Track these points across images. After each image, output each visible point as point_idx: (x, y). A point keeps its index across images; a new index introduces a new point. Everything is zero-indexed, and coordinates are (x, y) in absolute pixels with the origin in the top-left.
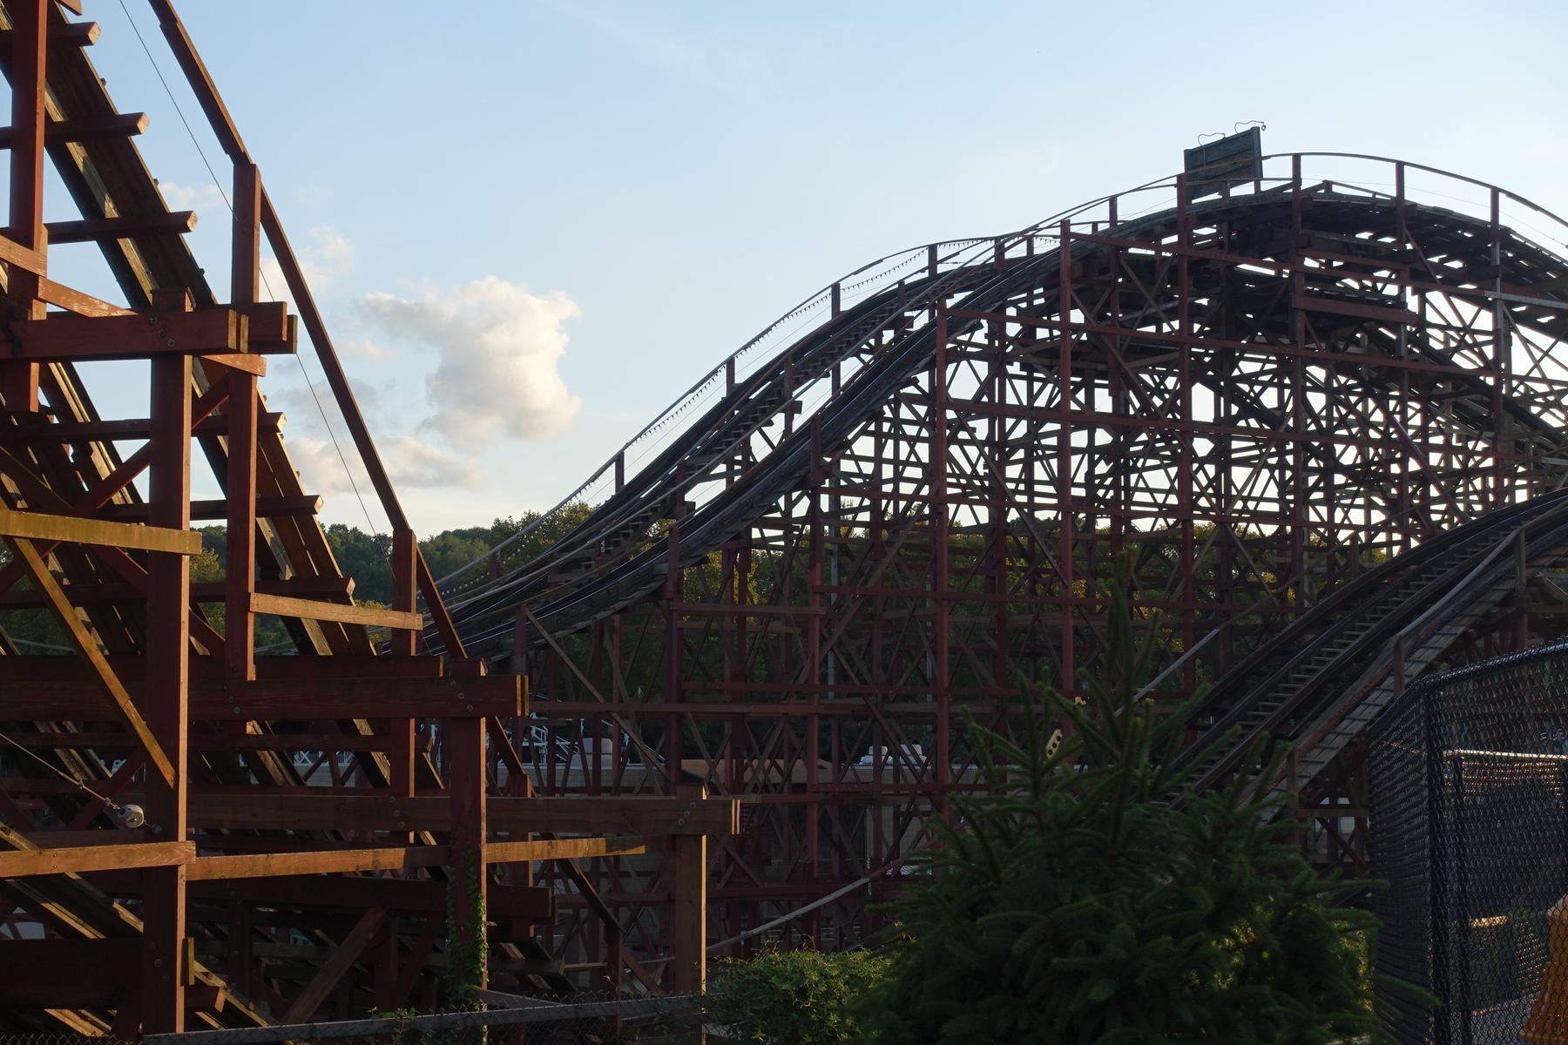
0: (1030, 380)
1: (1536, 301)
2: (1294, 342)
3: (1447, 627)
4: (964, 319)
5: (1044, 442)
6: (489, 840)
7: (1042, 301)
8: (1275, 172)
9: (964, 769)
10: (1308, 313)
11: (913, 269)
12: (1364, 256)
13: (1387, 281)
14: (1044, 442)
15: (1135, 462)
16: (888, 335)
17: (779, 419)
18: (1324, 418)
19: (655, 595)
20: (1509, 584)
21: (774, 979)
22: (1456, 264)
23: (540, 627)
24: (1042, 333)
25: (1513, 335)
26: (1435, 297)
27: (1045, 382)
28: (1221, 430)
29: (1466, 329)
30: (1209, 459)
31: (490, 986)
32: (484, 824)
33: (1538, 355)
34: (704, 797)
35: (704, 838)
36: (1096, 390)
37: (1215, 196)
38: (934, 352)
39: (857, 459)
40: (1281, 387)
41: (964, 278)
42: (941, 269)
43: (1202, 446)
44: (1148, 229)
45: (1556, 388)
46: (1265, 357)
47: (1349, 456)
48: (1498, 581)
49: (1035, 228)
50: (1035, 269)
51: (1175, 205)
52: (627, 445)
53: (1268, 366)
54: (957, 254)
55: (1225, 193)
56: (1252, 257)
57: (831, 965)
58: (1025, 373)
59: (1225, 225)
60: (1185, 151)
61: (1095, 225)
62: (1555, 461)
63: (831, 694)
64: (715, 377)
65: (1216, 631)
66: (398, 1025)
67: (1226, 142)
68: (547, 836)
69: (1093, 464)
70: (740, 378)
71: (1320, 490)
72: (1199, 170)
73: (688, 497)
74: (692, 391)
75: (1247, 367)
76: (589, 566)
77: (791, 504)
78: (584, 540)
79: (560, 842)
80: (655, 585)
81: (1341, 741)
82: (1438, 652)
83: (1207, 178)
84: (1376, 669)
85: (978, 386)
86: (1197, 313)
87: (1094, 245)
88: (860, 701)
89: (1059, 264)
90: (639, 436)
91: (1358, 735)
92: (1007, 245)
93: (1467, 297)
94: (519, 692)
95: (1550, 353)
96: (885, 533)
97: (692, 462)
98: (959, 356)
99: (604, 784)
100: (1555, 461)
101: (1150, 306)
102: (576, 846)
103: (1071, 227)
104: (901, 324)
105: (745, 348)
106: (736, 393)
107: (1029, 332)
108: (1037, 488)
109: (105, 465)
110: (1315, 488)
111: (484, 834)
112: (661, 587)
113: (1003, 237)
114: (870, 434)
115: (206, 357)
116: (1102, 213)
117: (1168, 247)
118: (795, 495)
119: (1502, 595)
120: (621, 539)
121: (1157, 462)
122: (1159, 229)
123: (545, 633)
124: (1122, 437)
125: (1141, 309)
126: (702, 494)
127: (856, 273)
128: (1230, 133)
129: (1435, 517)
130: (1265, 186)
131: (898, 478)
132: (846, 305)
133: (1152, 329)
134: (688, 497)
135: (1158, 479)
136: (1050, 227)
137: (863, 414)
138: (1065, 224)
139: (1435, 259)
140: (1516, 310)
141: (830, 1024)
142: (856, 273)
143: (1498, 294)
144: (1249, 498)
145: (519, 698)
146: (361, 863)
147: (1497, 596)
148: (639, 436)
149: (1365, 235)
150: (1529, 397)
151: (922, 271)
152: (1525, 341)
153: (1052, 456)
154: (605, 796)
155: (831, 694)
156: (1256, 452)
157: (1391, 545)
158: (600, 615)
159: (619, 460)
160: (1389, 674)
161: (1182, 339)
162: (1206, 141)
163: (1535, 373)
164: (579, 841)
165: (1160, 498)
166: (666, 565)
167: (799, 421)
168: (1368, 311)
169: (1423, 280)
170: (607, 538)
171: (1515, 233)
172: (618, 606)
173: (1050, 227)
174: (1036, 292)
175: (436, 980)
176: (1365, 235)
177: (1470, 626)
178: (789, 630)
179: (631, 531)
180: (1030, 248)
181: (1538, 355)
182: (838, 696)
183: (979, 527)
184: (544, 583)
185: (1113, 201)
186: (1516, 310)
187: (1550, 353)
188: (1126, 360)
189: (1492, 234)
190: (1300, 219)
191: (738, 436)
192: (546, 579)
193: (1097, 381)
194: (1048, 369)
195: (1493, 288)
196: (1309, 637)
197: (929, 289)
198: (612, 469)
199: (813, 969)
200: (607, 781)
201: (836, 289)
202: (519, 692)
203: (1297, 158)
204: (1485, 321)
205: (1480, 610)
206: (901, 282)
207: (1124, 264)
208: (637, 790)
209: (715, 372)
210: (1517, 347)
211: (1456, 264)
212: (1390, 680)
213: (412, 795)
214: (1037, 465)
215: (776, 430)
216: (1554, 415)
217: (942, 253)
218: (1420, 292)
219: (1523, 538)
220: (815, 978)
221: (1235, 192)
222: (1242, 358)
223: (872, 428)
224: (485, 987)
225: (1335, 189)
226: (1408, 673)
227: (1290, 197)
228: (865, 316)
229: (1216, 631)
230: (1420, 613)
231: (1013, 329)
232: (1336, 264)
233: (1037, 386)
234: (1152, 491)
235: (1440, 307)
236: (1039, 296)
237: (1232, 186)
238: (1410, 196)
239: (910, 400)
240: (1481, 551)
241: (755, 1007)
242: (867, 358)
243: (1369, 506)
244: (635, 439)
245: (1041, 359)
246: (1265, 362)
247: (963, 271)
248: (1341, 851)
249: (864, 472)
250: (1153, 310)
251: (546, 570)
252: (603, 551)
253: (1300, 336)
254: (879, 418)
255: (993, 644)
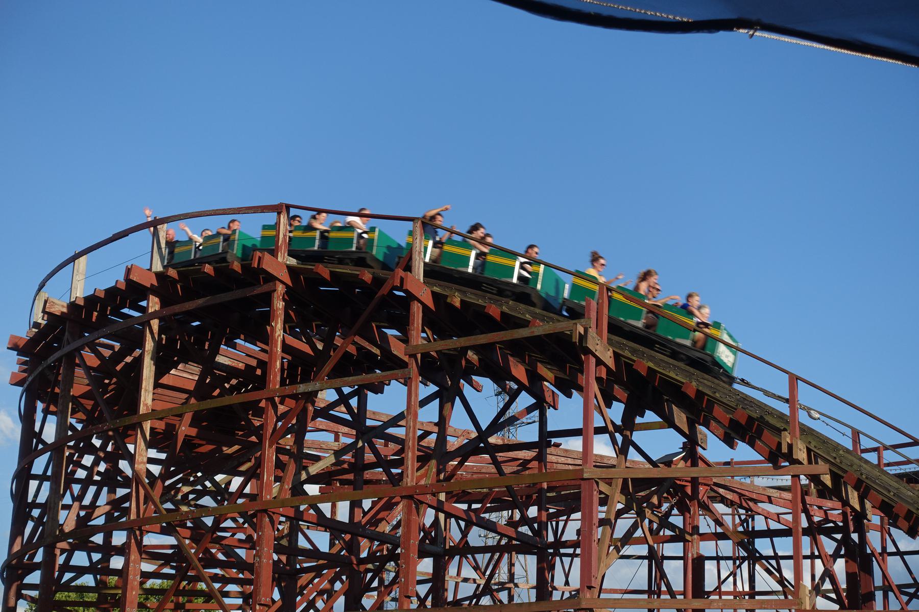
95: (646, 588)
103: (745, 590)
109: (702, 354)
115: (518, 543)
124: (82, 444)
187: (646, 588)
193: (653, 589)
248: (72, 443)
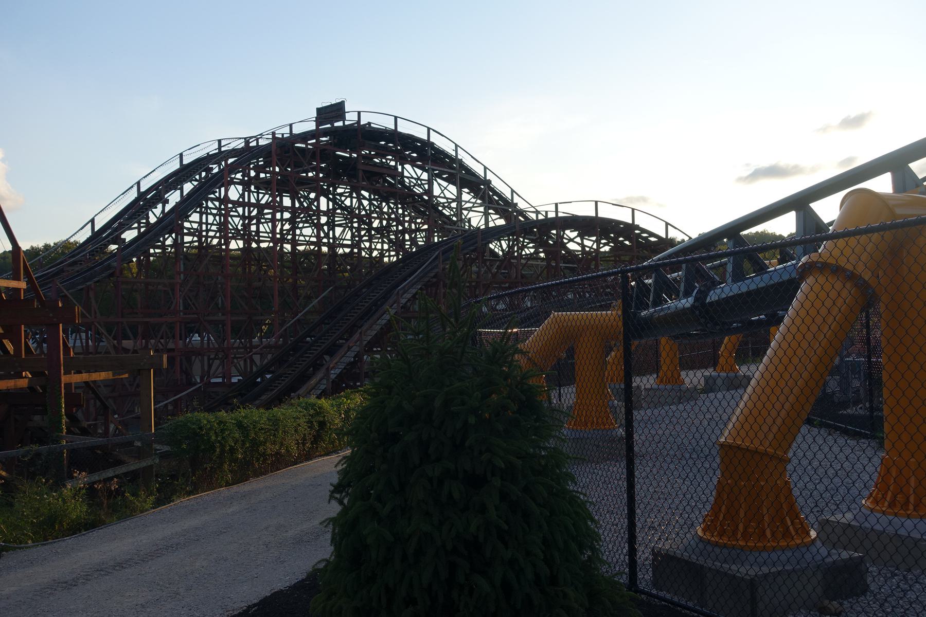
0: (258, 193)
1: (442, 169)
2: (358, 181)
3: (415, 286)
4: (233, 169)
5: (266, 216)
6: (65, 374)
7: (262, 163)
8: (351, 118)
9: (235, 342)
10: (363, 170)
11: (212, 149)
12: (383, 150)
13: (391, 160)
14: (266, 216)
15: (298, 225)
16: (204, 174)
17: (160, 206)
18: (361, 209)
19: (112, 275)
20: (436, 270)
21: (189, 424)
22: (415, 155)
23: (62, 288)
24: (262, 175)
25: (435, 182)
26: (408, 166)
27: (265, 194)
28: (330, 213)
29: (418, 179)
30: (326, 224)
31: (66, 433)
32: (62, 368)
33: (443, 188)
34: (152, 354)
35: (152, 370)
36: (284, 197)
37: (329, 126)
38: (223, 181)
39: (191, 222)
40: (352, 198)
41: (233, 152)
42: (223, 149)
43: (324, 220)
44: (304, 137)
45: (449, 200)
46: (345, 187)
47: (376, 224)
48: (431, 269)
49: (261, 134)
50: (262, 150)
51: (315, 128)
52: (96, 215)
53: (347, 190)
54: (230, 143)
55: (332, 125)
56: (343, 149)
57: (211, 417)
58: (256, 190)
59: (332, 137)
60: (317, 108)
61: (283, 135)
62: (449, 227)
63: (181, 314)
64: (132, 189)
65: (331, 288)
66: (31, 451)
67: (332, 106)
68: (89, 372)
69: (282, 225)
70: (143, 189)
71: (367, 236)
72: (322, 115)
73: (123, 236)
74: (123, 194)
75: (339, 191)
76: (81, 264)
77: (165, 240)
78: (79, 253)
79: (93, 374)
80: (111, 271)
81: (378, 328)
82: (412, 294)
83: (325, 119)
84: (391, 301)
85: (239, 196)
86: (322, 170)
87: (284, 142)
88: (196, 316)
89: (271, 149)
90: (101, 211)
91: (385, 325)
92: (250, 141)
93: (419, 167)
94: (77, 313)
96: (203, 251)
97: (124, 222)
98: (232, 182)
99: (90, 351)
100: (449, 227)
101: (306, 166)
102: (100, 375)
104: (209, 170)
105: (144, 177)
106: (141, 195)
107: (257, 175)
108: (261, 234)
110: (365, 235)
111: (62, 371)
112: (114, 272)
113: (248, 138)
114: (197, 212)
116: (287, 130)
117: (311, 144)
118: (166, 236)
119: (434, 274)
120: (95, 253)
121: (308, 225)
122: (309, 137)
123: (65, 291)
125: (302, 167)
126: (129, 235)
127: (189, 149)
128: (333, 102)
129: (407, 247)
130: (347, 123)
131: (207, 231)
132: (185, 162)
133: (305, 175)
134: (123, 236)
135: (308, 231)
136: (267, 134)
137: (195, 204)
138: (274, 134)
139: (407, 153)
140: (435, 172)
141: (212, 440)
142: (189, 149)
143: (430, 166)
144: (341, 239)
145: (77, 316)
146: (9, 385)
147: (432, 275)
148: (101, 211)
149: (383, 143)
150: (439, 204)
151: (216, 150)
152: (439, 184)
153: (269, 222)
154: (91, 356)
155: (181, 314)
156: (344, 222)
157: (391, 258)
158: (88, 283)
159: (92, 221)
160: (395, 303)
161: (316, 179)
162: (324, 105)
163: (442, 195)
164: (101, 373)
165: (307, 239)
166: (115, 263)
167: (168, 208)
168: (384, 171)
169: (403, 160)
170: (89, 252)
171: (435, 144)
172: (96, 279)
173: (267, 134)
174: (260, 160)
175: (30, 432)
176: (383, 143)
177: (423, 286)
178: (166, 289)
179: (99, 250)
180: (258, 143)
181: (443, 188)
182: (185, 314)
183: (239, 249)
184: (62, 271)
185: (291, 125)
186: (435, 172)
188: (297, 186)
189: (427, 144)
190: (360, 136)
191: (143, 212)
192: (63, 269)
193: (284, 194)
194: (266, 189)
195: (428, 164)
196: (364, 290)
197: (219, 156)
198: (90, 224)
199: (204, 419)
200: (91, 350)
201: (181, 155)
202: (77, 313)
203: (359, 113)
204: (425, 176)
205: (426, 279)
206: (208, 154)
207: (295, 150)
208: (103, 353)
209: (132, 187)
210: (435, 185)
211: (415, 155)
212: (395, 305)
213: (23, 357)
214: (261, 225)
215: (158, 210)
216: (446, 210)
217: (223, 143)
218: (402, 165)
219: (441, 254)
220: (205, 422)
221: (336, 124)
222: (339, 187)
223: (198, 210)
224: (64, 434)
225: (372, 125)
226: (402, 302)
227: (356, 128)
228: (194, 166)
229: (331, 288)
230: (405, 281)
231: (253, 174)
232: (372, 153)
233: (261, 196)
234: (304, 236)
235: (409, 170)
236: (261, 161)
237: (335, 122)
238: (400, 129)
239: (212, 200)
240: (426, 258)
241: (182, 435)
242: (195, 183)
243: (383, 242)
244: (99, 213)
245: (263, 185)
246: (345, 189)
247: (233, 150)
249: (194, 227)
250: (306, 168)
251: (63, 266)
252: (88, 258)
253: (360, 179)
254: (201, 206)
255: (245, 294)
